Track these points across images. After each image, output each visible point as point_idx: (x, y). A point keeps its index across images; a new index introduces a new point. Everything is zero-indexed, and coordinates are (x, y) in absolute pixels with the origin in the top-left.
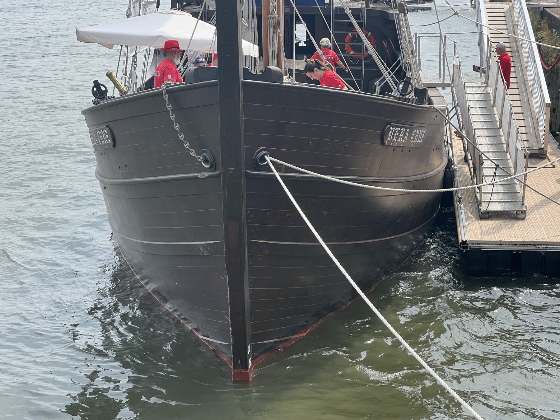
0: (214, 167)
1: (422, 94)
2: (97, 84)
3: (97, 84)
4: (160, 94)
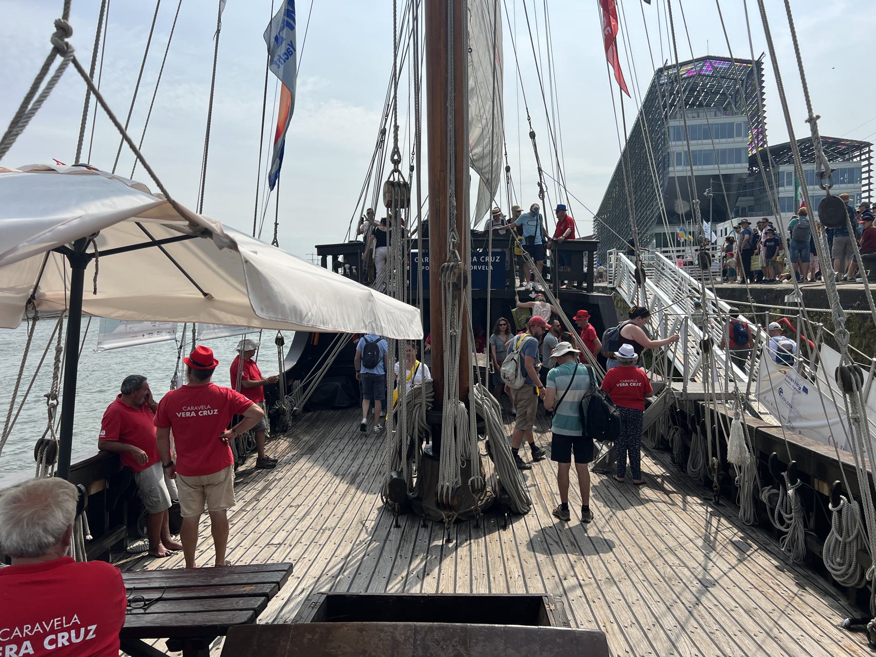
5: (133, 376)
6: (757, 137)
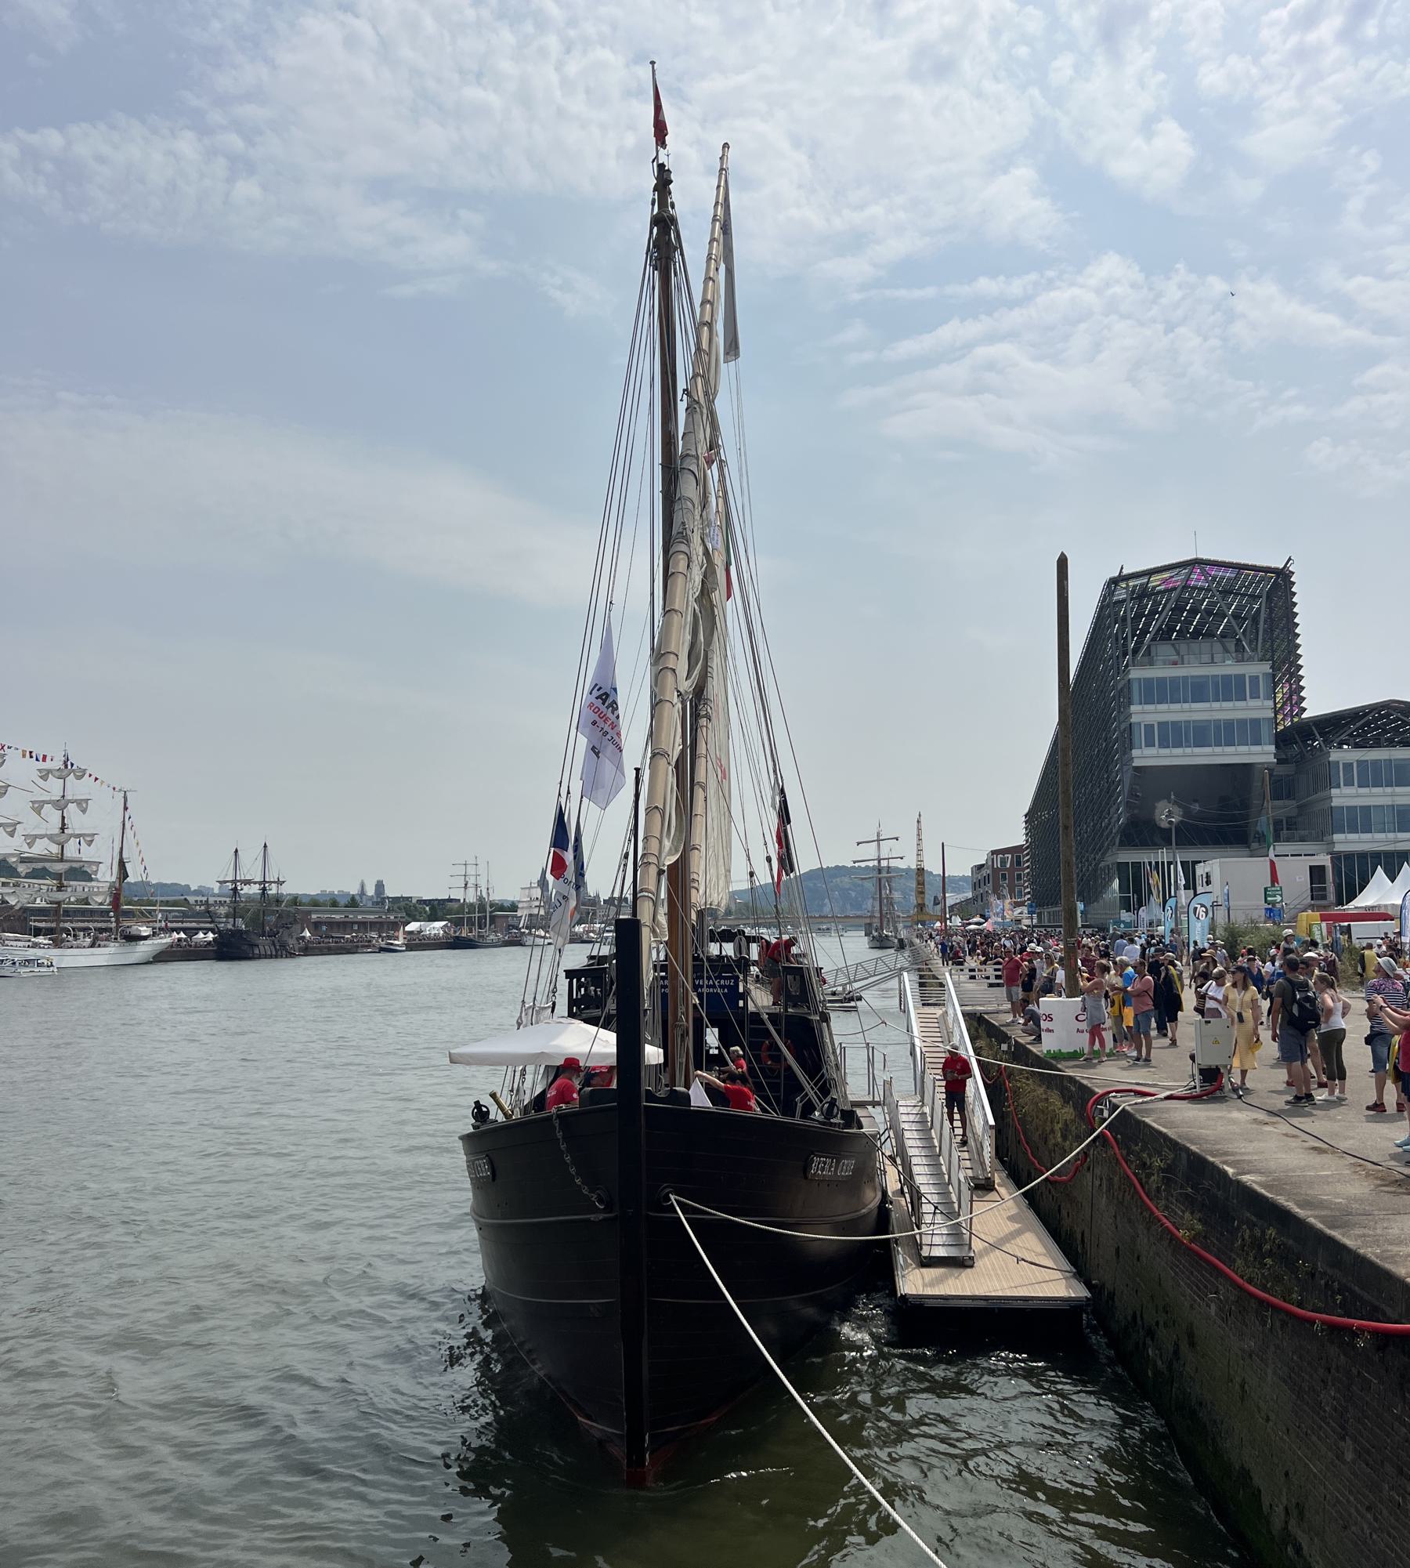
0: (609, 1208)
1: (850, 1118)
2: (478, 1105)
3: (478, 1105)
4: (549, 1119)
5: (1030, 817)
6: (1290, 698)
